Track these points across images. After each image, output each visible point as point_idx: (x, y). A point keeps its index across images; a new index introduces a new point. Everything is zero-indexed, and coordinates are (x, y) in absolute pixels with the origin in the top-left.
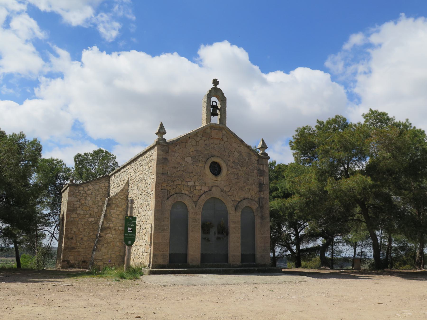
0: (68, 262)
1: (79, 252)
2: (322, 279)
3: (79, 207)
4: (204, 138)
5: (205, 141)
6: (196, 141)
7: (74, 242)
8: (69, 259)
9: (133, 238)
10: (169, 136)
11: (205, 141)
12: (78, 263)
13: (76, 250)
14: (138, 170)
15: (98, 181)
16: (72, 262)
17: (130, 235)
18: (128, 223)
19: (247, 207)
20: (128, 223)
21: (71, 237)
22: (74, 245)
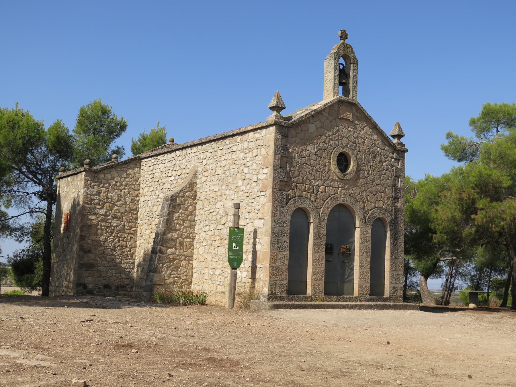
0: (85, 286)
1: (99, 271)
2: (427, 313)
3: (99, 204)
4: (331, 118)
5: (331, 122)
6: (321, 122)
7: (92, 256)
8: (86, 282)
9: (240, 257)
10: (297, 112)
11: (331, 122)
12: (99, 288)
13: (96, 269)
14: (223, 158)
15: (125, 166)
16: (90, 286)
17: (236, 253)
18: (234, 237)
19: (379, 219)
20: (234, 237)
21: (88, 249)
22: (92, 261)
